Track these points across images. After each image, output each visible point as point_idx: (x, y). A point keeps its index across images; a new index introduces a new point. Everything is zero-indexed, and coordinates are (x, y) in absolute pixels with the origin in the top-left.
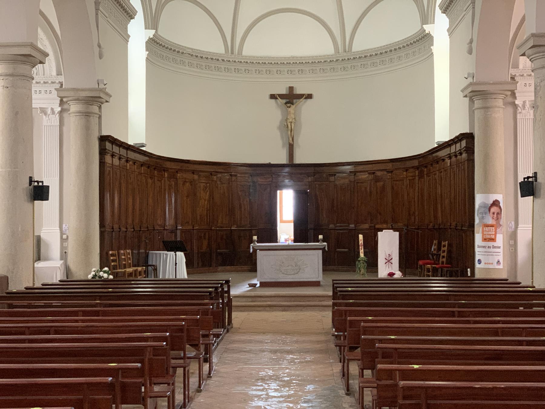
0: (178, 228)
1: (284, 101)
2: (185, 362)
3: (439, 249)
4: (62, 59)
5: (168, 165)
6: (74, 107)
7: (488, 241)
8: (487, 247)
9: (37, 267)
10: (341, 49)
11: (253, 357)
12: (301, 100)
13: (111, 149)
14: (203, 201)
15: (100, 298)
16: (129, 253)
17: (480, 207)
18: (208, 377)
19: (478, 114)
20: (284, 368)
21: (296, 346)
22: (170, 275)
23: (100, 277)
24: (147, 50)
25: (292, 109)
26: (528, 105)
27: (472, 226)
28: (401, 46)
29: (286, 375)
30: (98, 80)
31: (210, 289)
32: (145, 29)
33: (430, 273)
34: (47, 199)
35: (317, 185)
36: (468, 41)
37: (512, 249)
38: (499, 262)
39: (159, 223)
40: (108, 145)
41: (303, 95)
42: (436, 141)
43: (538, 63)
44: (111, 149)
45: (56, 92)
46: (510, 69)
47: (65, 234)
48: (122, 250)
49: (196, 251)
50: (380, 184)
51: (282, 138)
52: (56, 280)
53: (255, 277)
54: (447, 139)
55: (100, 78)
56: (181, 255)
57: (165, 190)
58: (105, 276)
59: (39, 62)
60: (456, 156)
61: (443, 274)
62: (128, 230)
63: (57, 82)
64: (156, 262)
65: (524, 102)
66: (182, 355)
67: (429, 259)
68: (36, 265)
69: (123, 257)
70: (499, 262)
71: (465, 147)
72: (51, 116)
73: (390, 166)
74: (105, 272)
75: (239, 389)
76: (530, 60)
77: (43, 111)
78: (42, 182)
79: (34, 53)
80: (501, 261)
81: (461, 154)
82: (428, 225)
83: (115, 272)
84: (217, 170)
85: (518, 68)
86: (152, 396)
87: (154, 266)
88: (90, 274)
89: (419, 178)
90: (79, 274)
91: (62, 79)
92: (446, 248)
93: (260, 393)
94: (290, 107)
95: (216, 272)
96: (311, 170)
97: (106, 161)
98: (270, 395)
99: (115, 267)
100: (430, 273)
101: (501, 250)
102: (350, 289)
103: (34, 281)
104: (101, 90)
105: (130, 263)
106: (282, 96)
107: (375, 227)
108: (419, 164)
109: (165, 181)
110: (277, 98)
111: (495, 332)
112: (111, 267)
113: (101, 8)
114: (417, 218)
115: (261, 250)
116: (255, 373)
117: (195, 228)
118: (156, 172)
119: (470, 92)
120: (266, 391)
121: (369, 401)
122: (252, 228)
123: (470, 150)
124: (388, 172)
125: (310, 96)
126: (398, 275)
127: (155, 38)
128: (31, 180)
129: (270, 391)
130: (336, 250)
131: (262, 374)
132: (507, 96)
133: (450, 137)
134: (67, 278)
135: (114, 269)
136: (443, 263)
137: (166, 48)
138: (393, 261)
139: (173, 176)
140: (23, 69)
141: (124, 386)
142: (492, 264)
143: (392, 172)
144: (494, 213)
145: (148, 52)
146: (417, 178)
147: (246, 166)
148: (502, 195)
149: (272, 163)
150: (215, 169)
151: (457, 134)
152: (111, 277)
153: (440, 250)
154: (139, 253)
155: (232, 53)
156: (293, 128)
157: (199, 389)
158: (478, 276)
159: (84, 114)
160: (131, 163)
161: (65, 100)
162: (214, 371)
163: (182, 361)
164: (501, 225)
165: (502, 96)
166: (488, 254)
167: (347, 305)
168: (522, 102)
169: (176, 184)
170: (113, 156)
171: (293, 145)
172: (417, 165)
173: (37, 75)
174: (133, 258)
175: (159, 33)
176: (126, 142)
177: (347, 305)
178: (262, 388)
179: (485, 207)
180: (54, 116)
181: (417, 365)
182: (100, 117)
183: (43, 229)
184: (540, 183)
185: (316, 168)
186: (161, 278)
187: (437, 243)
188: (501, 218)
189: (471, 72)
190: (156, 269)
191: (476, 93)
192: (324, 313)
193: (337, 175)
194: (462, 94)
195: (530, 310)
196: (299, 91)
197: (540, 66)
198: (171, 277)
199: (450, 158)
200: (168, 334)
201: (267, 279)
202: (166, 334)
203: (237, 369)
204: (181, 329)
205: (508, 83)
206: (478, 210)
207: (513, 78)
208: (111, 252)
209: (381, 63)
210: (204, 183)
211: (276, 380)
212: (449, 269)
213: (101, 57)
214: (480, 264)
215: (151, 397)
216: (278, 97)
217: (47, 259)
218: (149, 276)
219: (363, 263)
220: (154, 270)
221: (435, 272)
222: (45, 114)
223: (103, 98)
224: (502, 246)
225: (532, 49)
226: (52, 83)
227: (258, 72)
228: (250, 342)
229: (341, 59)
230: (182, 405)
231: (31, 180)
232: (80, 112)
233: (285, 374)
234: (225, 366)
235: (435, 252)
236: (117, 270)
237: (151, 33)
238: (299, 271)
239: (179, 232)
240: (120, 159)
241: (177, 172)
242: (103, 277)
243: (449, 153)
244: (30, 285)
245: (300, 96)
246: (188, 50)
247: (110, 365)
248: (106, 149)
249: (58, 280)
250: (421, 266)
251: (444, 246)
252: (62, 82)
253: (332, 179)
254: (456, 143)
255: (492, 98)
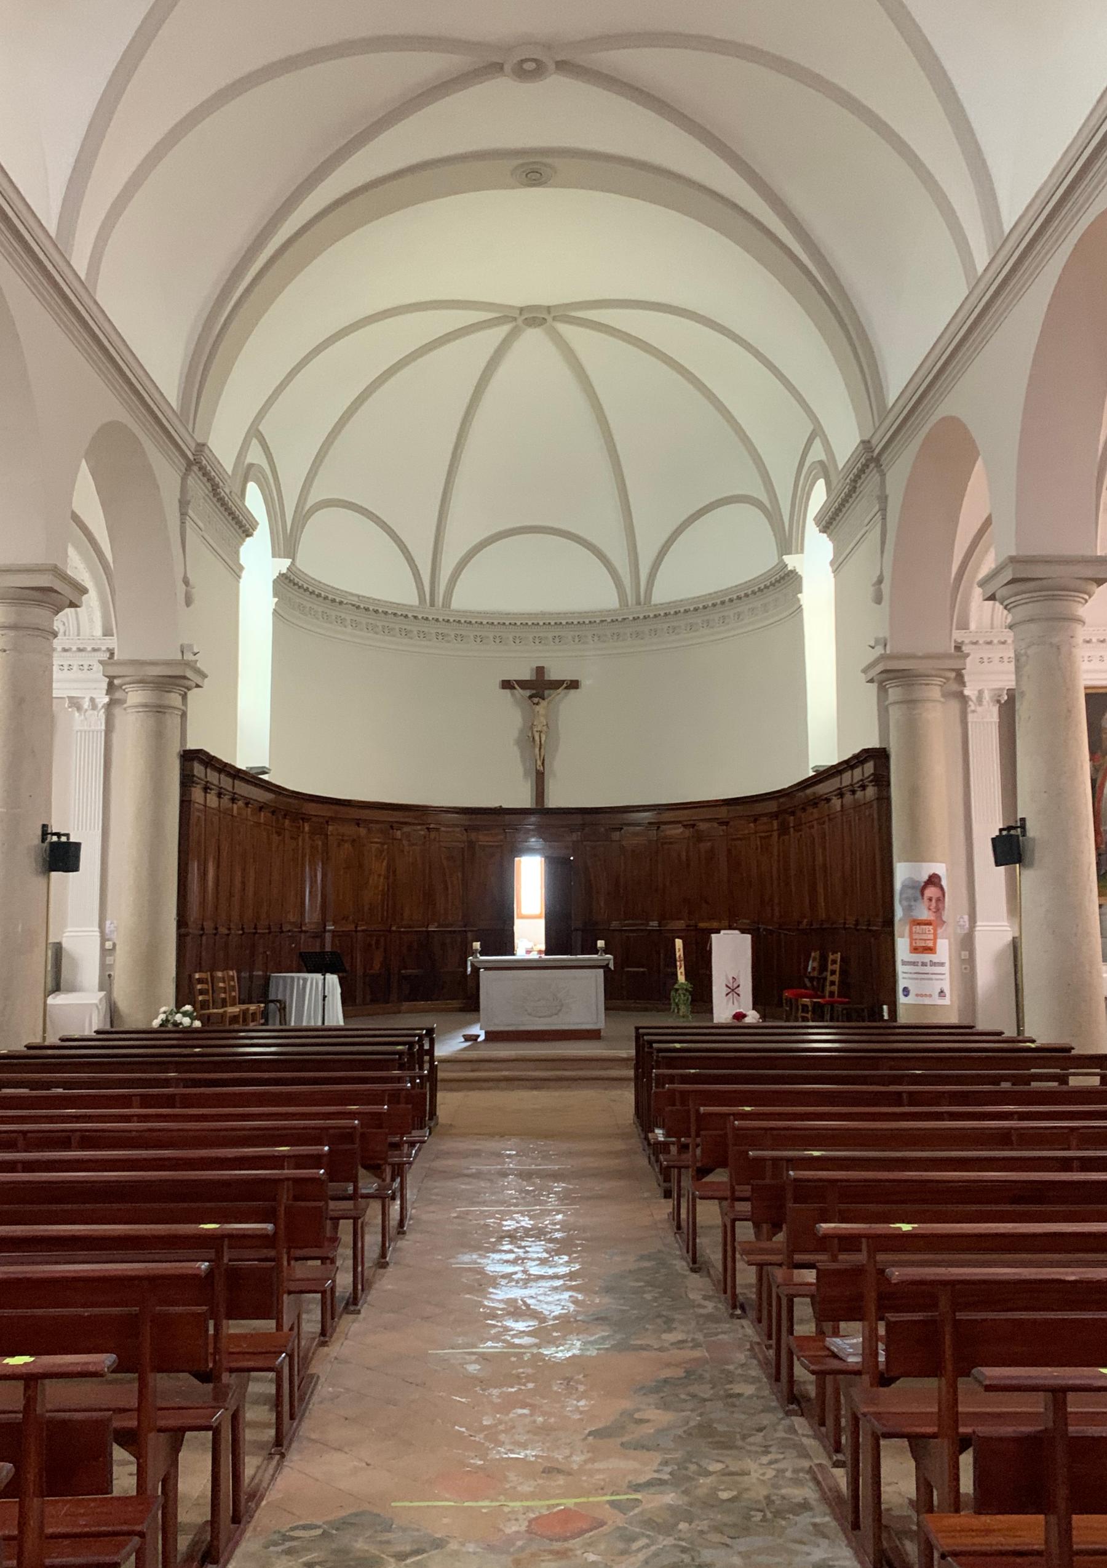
0: (328, 928)
1: (528, 693)
2: (356, 1208)
3: (823, 967)
4: (114, 604)
5: (311, 809)
6: (135, 696)
7: (922, 953)
8: (920, 964)
9: (52, 1005)
10: (631, 599)
11: (485, 1188)
12: (559, 691)
13: (202, 776)
14: (376, 877)
15: (178, 1067)
16: (233, 977)
17: (905, 887)
18: (399, 1233)
19: (895, 714)
20: (553, 1210)
21: (568, 1164)
22: (310, 1019)
23: (176, 1024)
24: (275, 595)
25: (541, 709)
26: (987, 696)
27: (889, 922)
28: (742, 594)
29: (558, 1227)
30: (182, 646)
31: (400, 1047)
32: (274, 556)
33: (809, 1015)
34: (75, 868)
35: (588, 848)
36: (875, 579)
37: (966, 968)
38: (942, 992)
39: (292, 918)
40: (198, 769)
41: (563, 682)
42: (811, 765)
43: (1022, 612)
44: (202, 776)
45: (101, 667)
46: (954, 631)
47: (108, 940)
48: (219, 970)
49: (360, 972)
50: (705, 846)
51: (524, 761)
52: (89, 1031)
53: (477, 1021)
54: (834, 761)
55: (186, 642)
56: (333, 979)
57: (304, 856)
58: (186, 1021)
59: (68, 602)
60: (853, 792)
61: (835, 1015)
62: (233, 932)
63: (104, 648)
64: (285, 995)
65: (981, 692)
66: (351, 1189)
67: (805, 987)
68: (51, 1000)
69: (221, 985)
70: (942, 992)
71: (872, 774)
72: (90, 712)
73: (723, 812)
74: (185, 1014)
75: (467, 1258)
76: (1005, 608)
77: (75, 703)
78: (67, 835)
79: (58, 585)
80: (947, 992)
81: (863, 787)
82: (799, 923)
83: (204, 1014)
84: (402, 820)
85: (968, 629)
86: (292, 1289)
87: (279, 1001)
88: (156, 1018)
89: (779, 836)
90: (134, 1018)
91: (112, 642)
92: (837, 967)
93: (510, 1269)
94: (537, 704)
95: (399, 1012)
96: (578, 819)
97: (193, 798)
98: (531, 1272)
99: (204, 1005)
100: (809, 1015)
101: (946, 970)
102: (678, 1046)
103: (44, 1031)
104: (187, 664)
105: (235, 997)
106: (523, 684)
107: (696, 926)
108: (779, 807)
109: (304, 840)
110: (514, 688)
111: (1004, 1139)
112: (198, 1006)
113: (190, 512)
114: (777, 909)
115: (486, 969)
116: (494, 1223)
117: (359, 929)
118: (287, 822)
119: (882, 672)
120: (523, 1263)
121: (750, 1286)
122: (467, 929)
123: (882, 780)
124: (721, 823)
125: (574, 685)
126: (752, 1017)
127: (290, 573)
128: (45, 832)
129: (530, 1263)
130: (623, 968)
131: (509, 1225)
132: (948, 679)
133: (839, 758)
134: (112, 1026)
135: (202, 1008)
136: (832, 994)
137: (311, 593)
138: (740, 990)
139: (319, 830)
140: (36, 615)
141: (234, 1276)
142: (930, 996)
143: (727, 823)
144: (930, 899)
145: (276, 599)
146: (775, 834)
147: (457, 813)
148: (944, 865)
149: (505, 806)
150: (398, 816)
151: (857, 751)
152: (197, 1024)
153: (826, 970)
154: (251, 977)
155: (432, 604)
156: (543, 742)
157: (383, 1260)
158: (903, 1018)
159: (155, 710)
160: (241, 803)
161: (116, 682)
162: (411, 1219)
163: (349, 1204)
164: (944, 922)
165: (938, 681)
166: (921, 976)
167: (685, 1079)
168: (976, 693)
169: (326, 844)
170: (206, 789)
171: (543, 774)
172: (775, 809)
173: (65, 635)
174: (239, 988)
175: (298, 563)
176: (233, 764)
177: (685, 1079)
178: (511, 1257)
179: (913, 888)
180: (96, 712)
181: (909, 1223)
182: (184, 715)
183: (69, 929)
184: (1033, 839)
185: (586, 816)
186: (293, 1024)
187: (818, 957)
188: (944, 907)
189: (881, 635)
190: (284, 1008)
191: (891, 675)
192: (615, 1093)
193: (625, 828)
194: (863, 678)
195: (1026, 1088)
196: (554, 675)
197: (1028, 618)
198: (312, 1024)
199: (841, 794)
200: (326, 1148)
201: (502, 1024)
202: (323, 1149)
203: (455, 1215)
204: (347, 1136)
205: (950, 656)
206: (901, 894)
207: (958, 648)
208: (197, 976)
209: (705, 625)
210: (376, 843)
211: (538, 1237)
212: (847, 1006)
213: (188, 601)
214: (906, 996)
215: (290, 1293)
216: (516, 686)
217: (73, 989)
218: (270, 1021)
219: (684, 995)
220: (279, 1010)
221: (818, 1013)
222: (79, 708)
223: (189, 679)
224: (946, 959)
225: (1009, 586)
226: (94, 650)
227: (479, 640)
228: (477, 1154)
229: (631, 618)
230: (349, 1298)
231: (45, 832)
232: (145, 706)
233: (555, 1224)
234: (432, 1208)
235: (815, 974)
236: (209, 1009)
237: (284, 564)
238: (560, 1010)
239: (328, 936)
240: (219, 795)
241: (327, 822)
242: (181, 1024)
243: (839, 786)
244: (37, 1040)
245: (556, 685)
246: (350, 598)
247: (203, 1229)
248: (194, 776)
249: (95, 1028)
250: (789, 1002)
251: (834, 962)
252: (114, 649)
253: (616, 835)
254: (852, 768)
255: (921, 684)
